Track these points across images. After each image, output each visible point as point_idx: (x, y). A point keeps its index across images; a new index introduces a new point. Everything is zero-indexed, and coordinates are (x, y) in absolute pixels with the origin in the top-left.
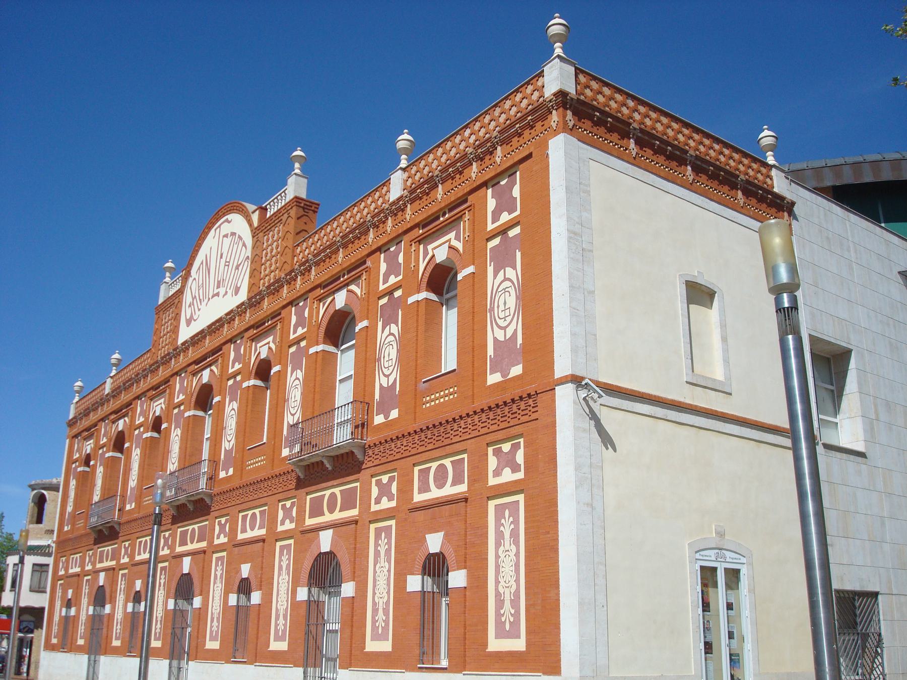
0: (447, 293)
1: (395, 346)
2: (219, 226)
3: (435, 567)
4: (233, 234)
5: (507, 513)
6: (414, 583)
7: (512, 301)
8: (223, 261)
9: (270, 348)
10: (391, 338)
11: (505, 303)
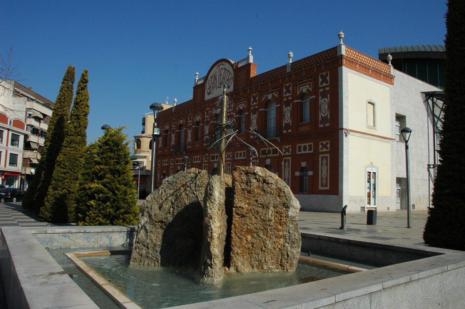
0: (305, 100)
1: (327, 104)
2: (219, 65)
4: (225, 69)
5: (287, 161)
6: (297, 174)
7: (326, 107)
8: (222, 77)
9: (244, 107)
10: (255, 118)
11: (324, 107)
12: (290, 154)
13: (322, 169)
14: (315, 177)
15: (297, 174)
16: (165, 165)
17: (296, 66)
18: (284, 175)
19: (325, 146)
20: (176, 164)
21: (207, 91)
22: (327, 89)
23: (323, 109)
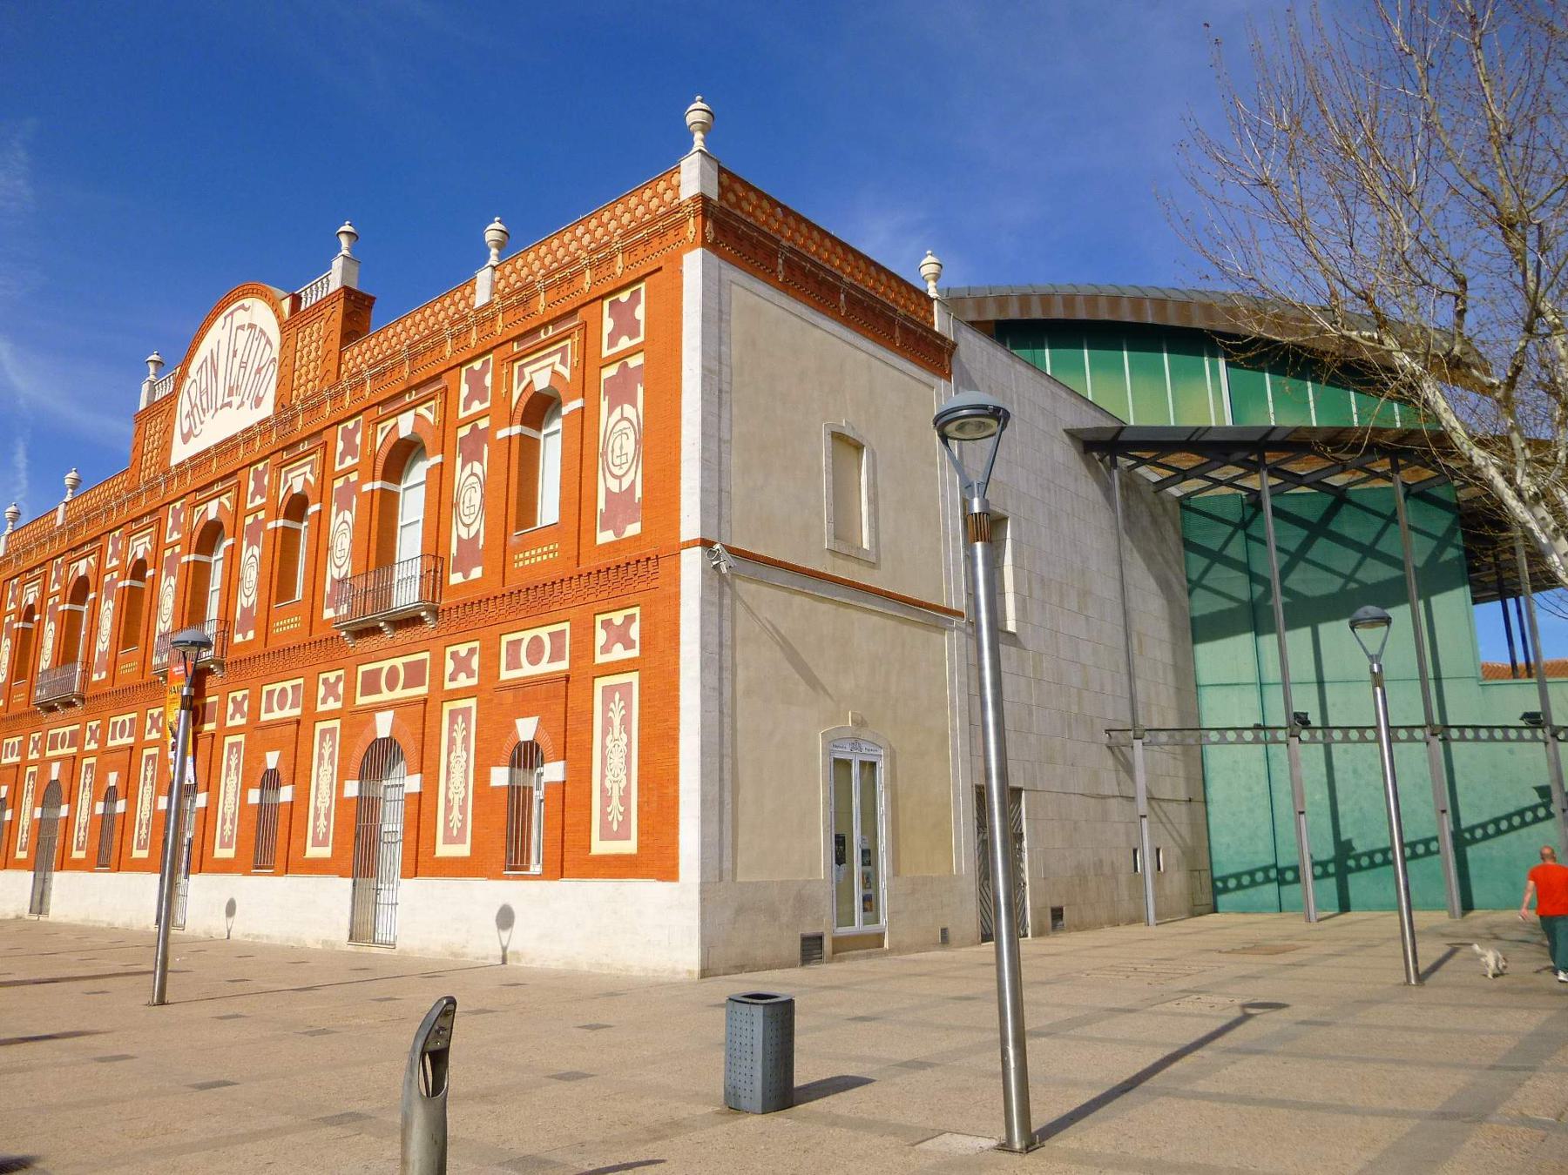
1: (632, 437)
2: (231, 314)
3: (527, 756)
4: (252, 326)
6: (500, 776)
7: (630, 446)
8: (237, 361)
12: (635, 653)
13: (449, 763)
14: (571, 801)
15: (500, 776)
16: (277, 714)
17: (395, 340)
18: (448, 788)
19: (462, 665)
20: (361, 700)
21: (180, 425)
22: (636, 361)
23: (614, 458)
